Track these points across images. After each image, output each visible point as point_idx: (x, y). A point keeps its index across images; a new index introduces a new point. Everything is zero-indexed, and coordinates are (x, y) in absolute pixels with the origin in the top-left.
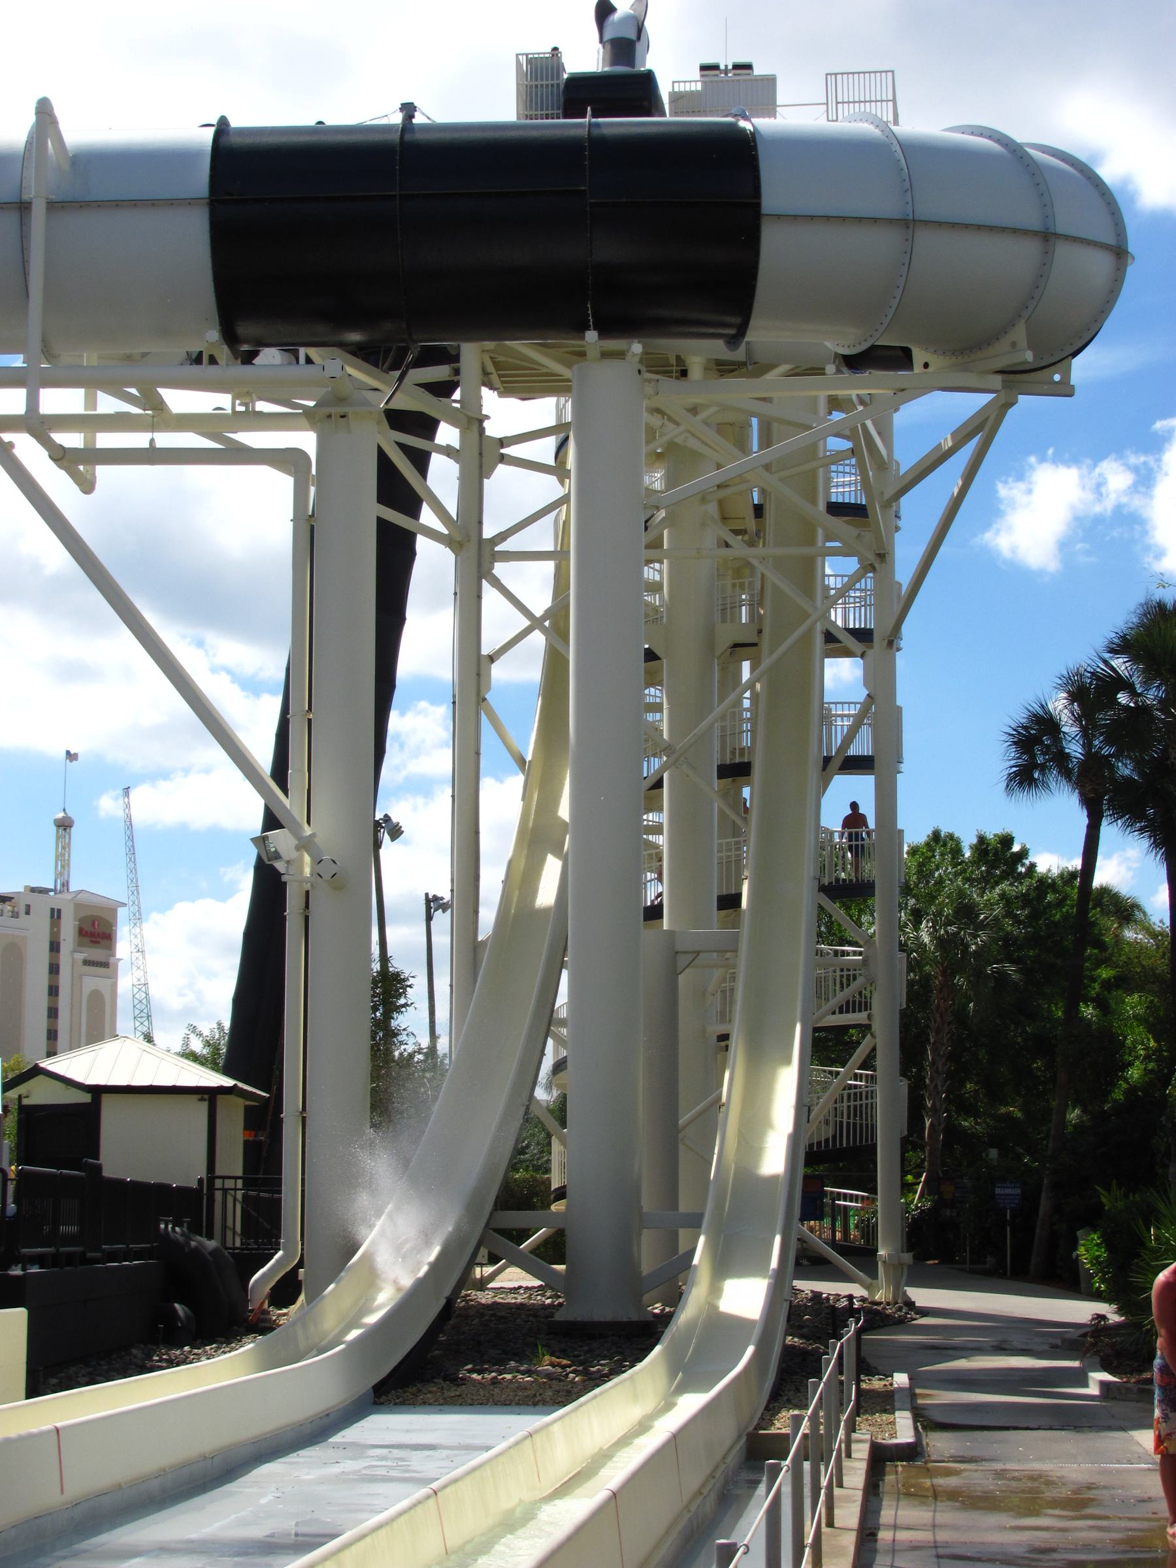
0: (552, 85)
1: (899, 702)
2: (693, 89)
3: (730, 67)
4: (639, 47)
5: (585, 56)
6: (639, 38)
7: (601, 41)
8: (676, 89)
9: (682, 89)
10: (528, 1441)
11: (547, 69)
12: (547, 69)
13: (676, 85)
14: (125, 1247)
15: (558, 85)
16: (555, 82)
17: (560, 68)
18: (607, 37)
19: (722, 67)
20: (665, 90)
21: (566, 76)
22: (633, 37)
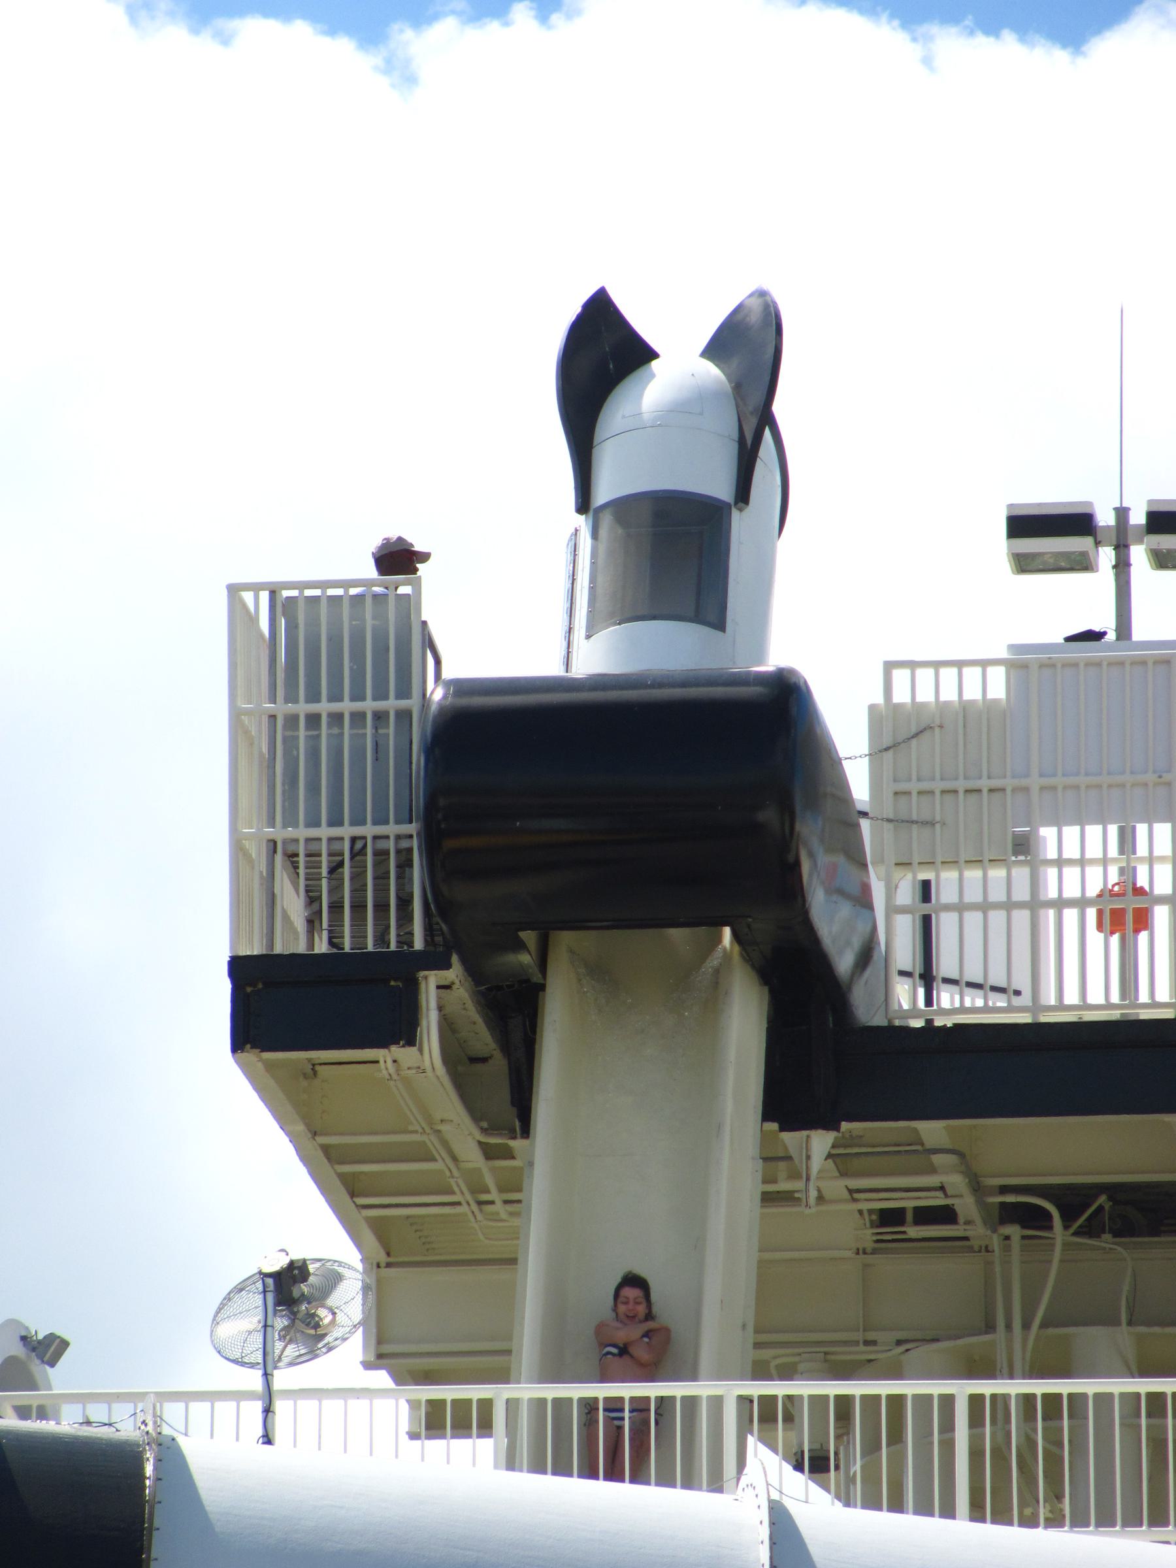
0: (358, 718)
1: (256, 32)
2: (972, 693)
3: (1138, 518)
4: (740, 524)
5: (519, 611)
6: (743, 493)
7: (583, 504)
8: (901, 695)
9: (925, 695)
10: (900, 739)
11: (335, 641)
12: (335, 641)
13: (901, 677)
14: (1163, 521)
15: (404, 716)
16: (392, 704)
17: (410, 642)
18: (603, 494)
19: (1105, 518)
20: (846, 729)
21: (437, 694)
22: (721, 488)
